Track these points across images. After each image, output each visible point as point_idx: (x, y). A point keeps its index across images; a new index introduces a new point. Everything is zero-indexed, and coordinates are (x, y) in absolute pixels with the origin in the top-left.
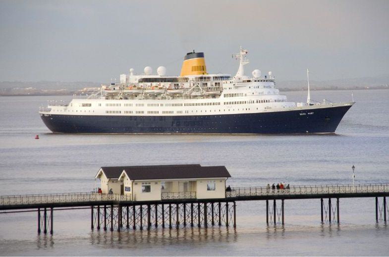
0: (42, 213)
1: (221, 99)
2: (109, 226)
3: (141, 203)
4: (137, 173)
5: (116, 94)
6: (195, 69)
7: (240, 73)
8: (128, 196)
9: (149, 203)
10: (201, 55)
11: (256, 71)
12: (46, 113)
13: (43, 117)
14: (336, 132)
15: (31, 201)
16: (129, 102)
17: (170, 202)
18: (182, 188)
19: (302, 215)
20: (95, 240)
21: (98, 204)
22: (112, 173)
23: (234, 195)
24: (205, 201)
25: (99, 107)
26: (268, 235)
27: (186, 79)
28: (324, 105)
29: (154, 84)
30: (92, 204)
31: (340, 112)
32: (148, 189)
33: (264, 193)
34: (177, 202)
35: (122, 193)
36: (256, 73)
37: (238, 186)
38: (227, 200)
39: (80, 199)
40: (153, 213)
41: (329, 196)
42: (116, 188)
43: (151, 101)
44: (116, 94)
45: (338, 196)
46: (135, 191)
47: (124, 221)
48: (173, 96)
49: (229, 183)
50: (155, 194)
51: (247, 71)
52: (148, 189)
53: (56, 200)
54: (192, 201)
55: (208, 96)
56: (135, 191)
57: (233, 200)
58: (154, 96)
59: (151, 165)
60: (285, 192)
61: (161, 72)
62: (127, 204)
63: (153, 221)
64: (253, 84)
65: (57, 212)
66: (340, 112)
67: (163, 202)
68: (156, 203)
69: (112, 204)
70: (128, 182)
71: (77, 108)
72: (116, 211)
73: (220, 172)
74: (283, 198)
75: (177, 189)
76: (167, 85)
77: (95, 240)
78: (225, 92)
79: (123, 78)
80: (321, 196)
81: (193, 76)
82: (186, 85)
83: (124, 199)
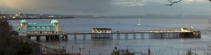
4: (98, 29)
17: (103, 34)
19: (139, 36)
32: (99, 32)
46: (98, 32)
50: (101, 32)
52: (99, 32)
62: (96, 34)
70: (96, 31)
72: (171, 37)
73: (110, 29)
75: (104, 32)
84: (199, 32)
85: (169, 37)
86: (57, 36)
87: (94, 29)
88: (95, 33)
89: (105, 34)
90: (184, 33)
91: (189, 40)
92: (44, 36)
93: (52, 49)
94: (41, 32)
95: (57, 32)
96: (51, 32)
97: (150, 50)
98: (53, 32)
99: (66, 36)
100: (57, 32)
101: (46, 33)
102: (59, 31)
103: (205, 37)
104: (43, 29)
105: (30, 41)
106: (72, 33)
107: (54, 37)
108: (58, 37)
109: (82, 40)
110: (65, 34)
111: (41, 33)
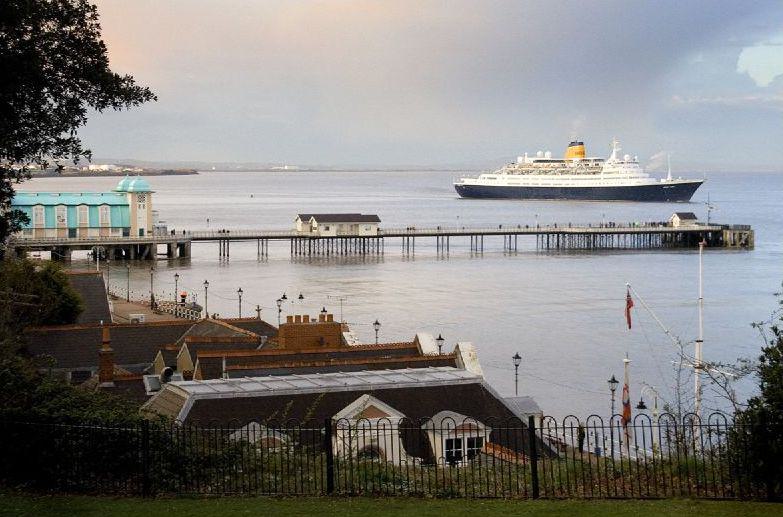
0: (540, 239)
1: (602, 176)
2: (302, 252)
3: (323, 238)
4: (321, 218)
5: (515, 171)
6: (577, 153)
7: (613, 156)
8: (315, 233)
9: (328, 238)
10: (581, 144)
11: (626, 156)
12: (459, 184)
13: (456, 186)
14: (692, 199)
15: (254, 235)
16: (526, 176)
17: (342, 237)
18: (349, 228)
19: (425, 247)
20: (294, 261)
21: (296, 237)
22: (305, 218)
23: (382, 233)
24: (364, 237)
25: (502, 180)
26: (403, 260)
27: (571, 161)
28: (679, 181)
29: (546, 164)
30: (292, 238)
31: (694, 187)
32: (327, 229)
33: (402, 233)
34: (346, 237)
35: (311, 231)
36: (627, 157)
37: (385, 225)
38: (378, 237)
39: (285, 234)
40: (330, 244)
41: (477, 234)
42: (308, 227)
43: (543, 176)
44: (515, 171)
45: (448, 235)
46: (321, 230)
47: (312, 249)
48: (562, 172)
49: (380, 225)
50: (332, 232)
51: (620, 155)
52: (327, 229)
53: (270, 234)
54: (356, 237)
55: (589, 173)
56: (321, 230)
57: (382, 237)
58: (546, 173)
59: (329, 213)
60: (416, 232)
61: (548, 156)
62: (314, 238)
63: (330, 249)
64: (626, 165)
65: (270, 242)
66: (694, 187)
67: (337, 237)
68: (332, 238)
69: (304, 237)
70: (315, 224)
71: (483, 181)
72: (307, 242)
73: (374, 219)
74: (414, 236)
75: (346, 229)
76: (557, 164)
77: (294, 261)
78: (604, 171)
79: (520, 159)
80: (472, 234)
81: (577, 159)
82: (572, 165)
83: (312, 235)
84: (747, 228)
85: (513, 246)
86: (143, 247)
87: (305, 218)
88: (309, 234)
89: (351, 237)
90: (685, 233)
91: (701, 261)
92: (45, 249)
93: (138, 303)
94: (72, 232)
95: (141, 231)
96: (115, 229)
97: (632, 296)
98: (126, 233)
99: (184, 249)
100: (141, 231)
101: (95, 234)
102: (154, 228)
103: (767, 242)
104: (81, 218)
105: (386, 480)
106: (458, 231)
107: (132, 252)
108: (149, 252)
109: (213, 265)
110: (179, 236)
111: (75, 236)
